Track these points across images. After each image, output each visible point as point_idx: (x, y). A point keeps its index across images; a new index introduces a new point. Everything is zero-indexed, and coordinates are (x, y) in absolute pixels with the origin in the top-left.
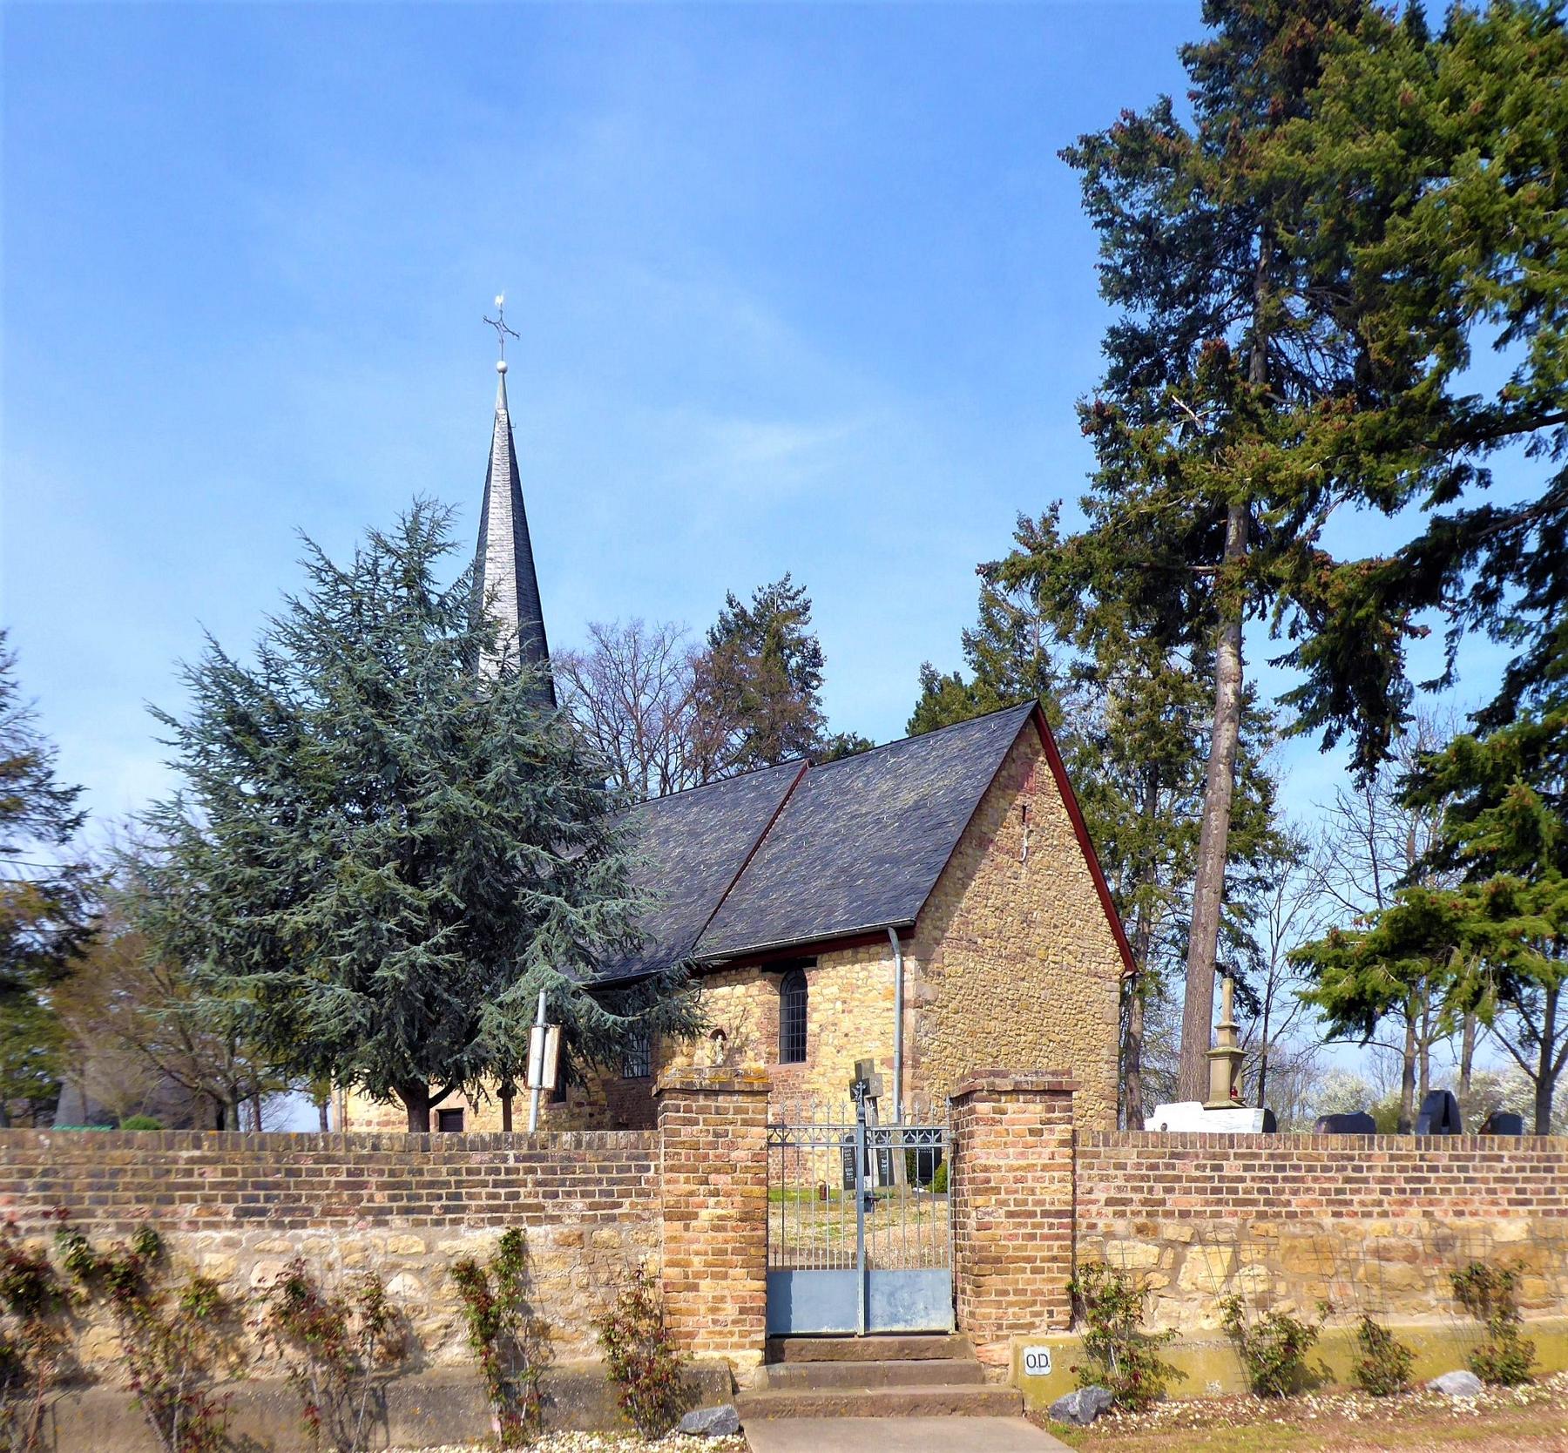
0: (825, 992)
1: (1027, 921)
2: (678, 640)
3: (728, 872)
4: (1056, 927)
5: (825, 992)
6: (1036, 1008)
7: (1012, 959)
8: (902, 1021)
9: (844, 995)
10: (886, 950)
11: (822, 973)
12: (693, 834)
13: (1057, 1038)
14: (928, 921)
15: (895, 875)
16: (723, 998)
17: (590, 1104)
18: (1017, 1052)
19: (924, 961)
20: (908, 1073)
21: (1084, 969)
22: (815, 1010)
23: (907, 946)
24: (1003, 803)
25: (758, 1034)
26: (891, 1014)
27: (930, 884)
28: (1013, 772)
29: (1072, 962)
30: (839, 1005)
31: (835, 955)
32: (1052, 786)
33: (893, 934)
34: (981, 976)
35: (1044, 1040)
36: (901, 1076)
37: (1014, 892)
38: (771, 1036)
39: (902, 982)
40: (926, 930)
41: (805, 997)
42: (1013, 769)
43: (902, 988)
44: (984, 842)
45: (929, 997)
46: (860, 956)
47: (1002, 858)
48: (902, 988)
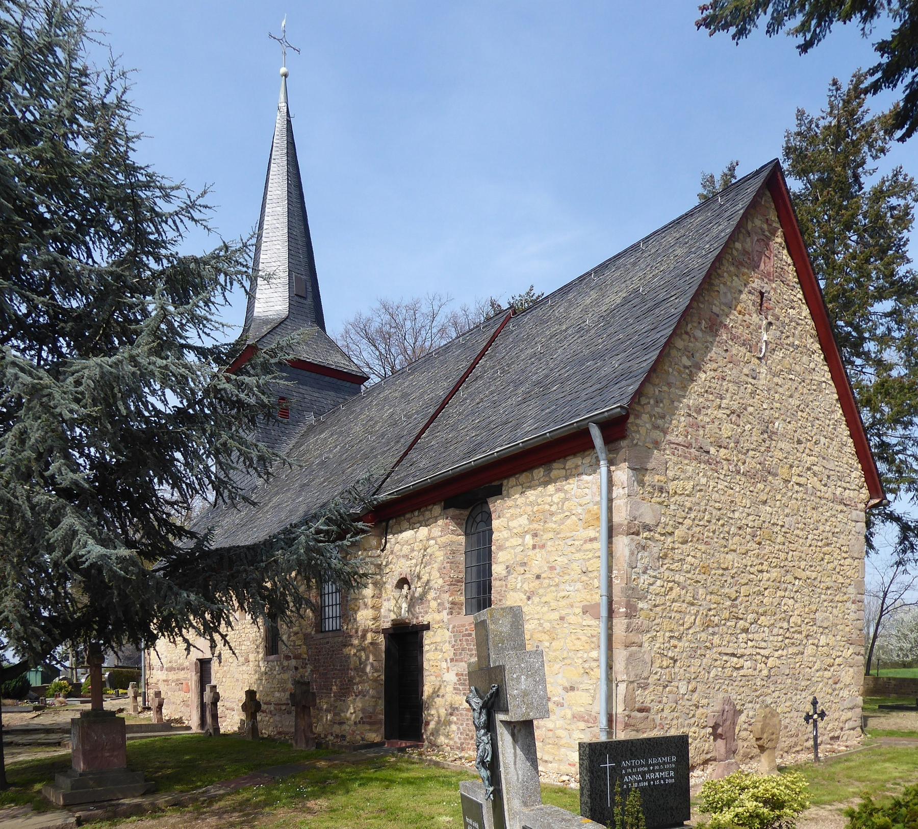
0: (512, 524)
1: (768, 432)
2: (444, 309)
3: (426, 415)
4: (799, 442)
5: (512, 524)
6: (780, 539)
7: (751, 476)
8: (610, 554)
9: (535, 526)
10: (587, 460)
11: (509, 502)
12: (405, 396)
13: (803, 575)
14: (645, 417)
15: (598, 369)
16: (406, 542)
17: (295, 658)
18: (760, 593)
19: (639, 470)
20: (620, 624)
21: (829, 495)
22: (501, 548)
23: (616, 451)
24: (737, 282)
25: (440, 581)
26: (596, 545)
27: (646, 365)
28: (748, 246)
29: (818, 485)
30: (528, 539)
31: (523, 477)
32: (791, 276)
33: (596, 433)
34: (715, 496)
35: (789, 578)
36: (610, 628)
37: (753, 394)
38: (454, 583)
39: (610, 500)
40: (641, 427)
41: (491, 532)
42: (749, 244)
43: (610, 509)
44: (714, 326)
45: (649, 520)
46: (554, 473)
47: (737, 350)
48: (610, 509)
